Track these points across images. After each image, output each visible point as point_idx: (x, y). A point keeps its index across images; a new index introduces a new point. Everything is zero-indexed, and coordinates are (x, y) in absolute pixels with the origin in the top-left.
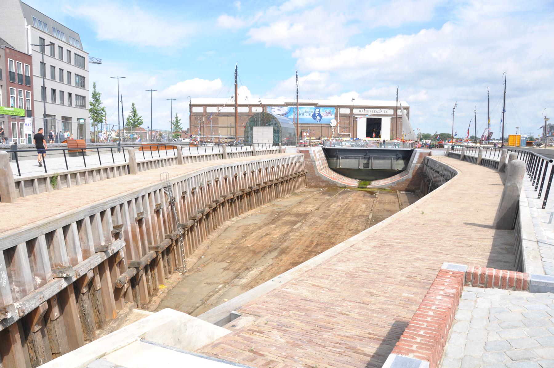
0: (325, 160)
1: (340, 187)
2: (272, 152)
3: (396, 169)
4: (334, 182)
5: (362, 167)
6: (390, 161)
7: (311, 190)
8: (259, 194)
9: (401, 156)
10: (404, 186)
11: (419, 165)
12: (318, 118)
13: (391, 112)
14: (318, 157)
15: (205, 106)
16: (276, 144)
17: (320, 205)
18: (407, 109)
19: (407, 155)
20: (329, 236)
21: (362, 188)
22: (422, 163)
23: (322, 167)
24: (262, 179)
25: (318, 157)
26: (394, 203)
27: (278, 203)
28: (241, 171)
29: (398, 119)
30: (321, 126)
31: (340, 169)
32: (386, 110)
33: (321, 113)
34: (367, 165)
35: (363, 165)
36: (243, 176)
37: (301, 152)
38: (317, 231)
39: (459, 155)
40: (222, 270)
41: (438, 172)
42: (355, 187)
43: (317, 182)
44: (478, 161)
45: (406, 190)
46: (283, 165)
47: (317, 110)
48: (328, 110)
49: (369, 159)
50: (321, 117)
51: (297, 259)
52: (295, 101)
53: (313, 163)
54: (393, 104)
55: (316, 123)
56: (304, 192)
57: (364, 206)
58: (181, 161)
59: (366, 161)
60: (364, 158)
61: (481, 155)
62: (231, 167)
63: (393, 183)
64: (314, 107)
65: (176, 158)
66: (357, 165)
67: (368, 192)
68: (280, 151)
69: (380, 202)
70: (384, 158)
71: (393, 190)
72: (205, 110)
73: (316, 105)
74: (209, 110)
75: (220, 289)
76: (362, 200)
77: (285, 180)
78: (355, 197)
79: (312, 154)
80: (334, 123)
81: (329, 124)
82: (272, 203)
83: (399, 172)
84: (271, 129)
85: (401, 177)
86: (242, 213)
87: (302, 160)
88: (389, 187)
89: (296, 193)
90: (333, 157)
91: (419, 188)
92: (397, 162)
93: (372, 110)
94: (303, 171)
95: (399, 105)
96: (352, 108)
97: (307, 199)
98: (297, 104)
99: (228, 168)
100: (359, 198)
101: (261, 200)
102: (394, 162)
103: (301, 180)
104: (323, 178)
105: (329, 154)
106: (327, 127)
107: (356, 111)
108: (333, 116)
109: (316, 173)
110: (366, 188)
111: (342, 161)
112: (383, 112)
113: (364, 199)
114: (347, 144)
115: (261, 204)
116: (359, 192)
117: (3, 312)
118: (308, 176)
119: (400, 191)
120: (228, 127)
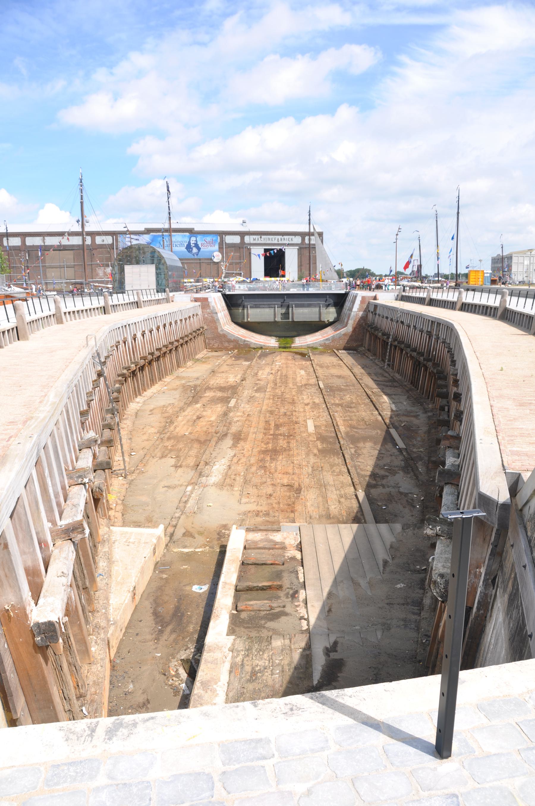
0: (226, 312)
1: (254, 348)
2: (158, 302)
3: (326, 320)
4: (245, 341)
5: (278, 319)
6: (317, 309)
7: (214, 354)
8: (159, 362)
9: (331, 301)
10: (343, 343)
11: (361, 313)
12: (195, 250)
13: (297, 240)
14: (219, 307)
15: (24, 235)
16: (160, 289)
17: (244, 374)
18: (320, 235)
19: (339, 301)
20: (285, 414)
21: (285, 348)
22: (365, 311)
23: (225, 321)
24: (161, 339)
25: (219, 307)
26: (339, 365)
27: (184, 375)
28: (140, 331)
29: (311, 249)
30: (200, 262)
31: (248, 322)
32: (291, 237)
33: (199, 243)
34: (286, 315)
35: (280, 316)
36: (142, 338)
37: (196, 300)
38: (264, 408)
39: (424, 299)
40: (173, 469)
41: (402, 322)
42: (274, 348)
43: (221, 342)
44: (458, 306)
45: (345, 349)
46: (181, 320)
47: (193, 239)
48: (209, 238)
49: (288, 307)
50: (199, 249)
51: (265, 446)
52: (167, 226)
53: (214, 315)
54: (304, 228)
55: (193, 257)
56: (209, 358)
57: (303, 372)
58: (62, 319)
59: (284, 311)
60: (282, 306)
61: (461, 298)
62: (129, 325)
63: (327, 339)
64: (187, 234)
65: (54, 315)
66: (273, 317)
67: (296, 353)
68: (167, 300)
69: (321, 366)
70: (309, 306)
71: (328, 349)
72: (24, 242)
73: (191, 231)
74: (30, 241)
75: (192, 492)
76: (295, 364)
77: (185, 341)
78: (283, 361)
79: (212, 304)
80: (217, 257)
81: (211, 259)
82: (176, 374)
83: (330, 324)
84: (152, 268)
85: (335, 331)
86: (145, 391)
87: (200, 312)
88: (321, 346)
89: (198, 360)
90: (238, 306)
91: (361, 345)
92: (327, 310)
93: (271, 237)
94: (203, 328)
95: (312, 230)
96: (242, 234)
97: (219, 366)
98: (170, 231)
99: (125, 326)
100: (289, 362)
101: (162, 370)
102: (324, 310)
103: (200, 340)
104: (229, 337)
105: (232, 302)
106: (209, 264)
107: (247, 239)
108: (217, 247)
109: (219, 330)
110: (290, 347)
111: (251, 311)
112: (287, 239)
113: (297, 363)
114: (242, 286)
115: (163, 377)
116: (284, 354)
117: (80, 530)
118: (208, 335)
119: (338, 350)
120: (60, 267)
